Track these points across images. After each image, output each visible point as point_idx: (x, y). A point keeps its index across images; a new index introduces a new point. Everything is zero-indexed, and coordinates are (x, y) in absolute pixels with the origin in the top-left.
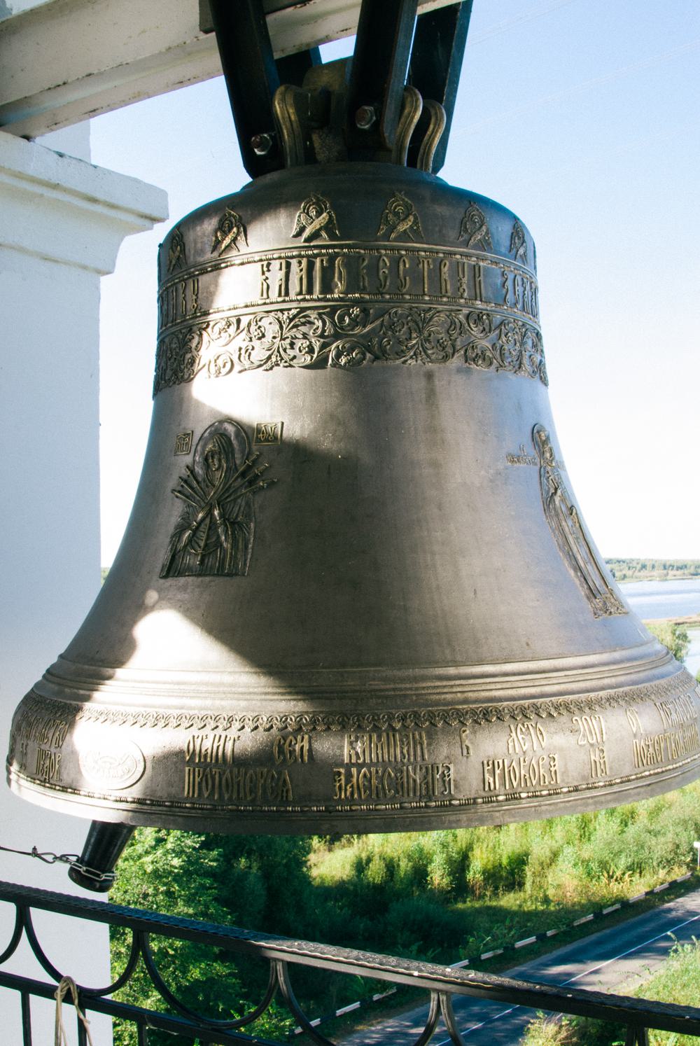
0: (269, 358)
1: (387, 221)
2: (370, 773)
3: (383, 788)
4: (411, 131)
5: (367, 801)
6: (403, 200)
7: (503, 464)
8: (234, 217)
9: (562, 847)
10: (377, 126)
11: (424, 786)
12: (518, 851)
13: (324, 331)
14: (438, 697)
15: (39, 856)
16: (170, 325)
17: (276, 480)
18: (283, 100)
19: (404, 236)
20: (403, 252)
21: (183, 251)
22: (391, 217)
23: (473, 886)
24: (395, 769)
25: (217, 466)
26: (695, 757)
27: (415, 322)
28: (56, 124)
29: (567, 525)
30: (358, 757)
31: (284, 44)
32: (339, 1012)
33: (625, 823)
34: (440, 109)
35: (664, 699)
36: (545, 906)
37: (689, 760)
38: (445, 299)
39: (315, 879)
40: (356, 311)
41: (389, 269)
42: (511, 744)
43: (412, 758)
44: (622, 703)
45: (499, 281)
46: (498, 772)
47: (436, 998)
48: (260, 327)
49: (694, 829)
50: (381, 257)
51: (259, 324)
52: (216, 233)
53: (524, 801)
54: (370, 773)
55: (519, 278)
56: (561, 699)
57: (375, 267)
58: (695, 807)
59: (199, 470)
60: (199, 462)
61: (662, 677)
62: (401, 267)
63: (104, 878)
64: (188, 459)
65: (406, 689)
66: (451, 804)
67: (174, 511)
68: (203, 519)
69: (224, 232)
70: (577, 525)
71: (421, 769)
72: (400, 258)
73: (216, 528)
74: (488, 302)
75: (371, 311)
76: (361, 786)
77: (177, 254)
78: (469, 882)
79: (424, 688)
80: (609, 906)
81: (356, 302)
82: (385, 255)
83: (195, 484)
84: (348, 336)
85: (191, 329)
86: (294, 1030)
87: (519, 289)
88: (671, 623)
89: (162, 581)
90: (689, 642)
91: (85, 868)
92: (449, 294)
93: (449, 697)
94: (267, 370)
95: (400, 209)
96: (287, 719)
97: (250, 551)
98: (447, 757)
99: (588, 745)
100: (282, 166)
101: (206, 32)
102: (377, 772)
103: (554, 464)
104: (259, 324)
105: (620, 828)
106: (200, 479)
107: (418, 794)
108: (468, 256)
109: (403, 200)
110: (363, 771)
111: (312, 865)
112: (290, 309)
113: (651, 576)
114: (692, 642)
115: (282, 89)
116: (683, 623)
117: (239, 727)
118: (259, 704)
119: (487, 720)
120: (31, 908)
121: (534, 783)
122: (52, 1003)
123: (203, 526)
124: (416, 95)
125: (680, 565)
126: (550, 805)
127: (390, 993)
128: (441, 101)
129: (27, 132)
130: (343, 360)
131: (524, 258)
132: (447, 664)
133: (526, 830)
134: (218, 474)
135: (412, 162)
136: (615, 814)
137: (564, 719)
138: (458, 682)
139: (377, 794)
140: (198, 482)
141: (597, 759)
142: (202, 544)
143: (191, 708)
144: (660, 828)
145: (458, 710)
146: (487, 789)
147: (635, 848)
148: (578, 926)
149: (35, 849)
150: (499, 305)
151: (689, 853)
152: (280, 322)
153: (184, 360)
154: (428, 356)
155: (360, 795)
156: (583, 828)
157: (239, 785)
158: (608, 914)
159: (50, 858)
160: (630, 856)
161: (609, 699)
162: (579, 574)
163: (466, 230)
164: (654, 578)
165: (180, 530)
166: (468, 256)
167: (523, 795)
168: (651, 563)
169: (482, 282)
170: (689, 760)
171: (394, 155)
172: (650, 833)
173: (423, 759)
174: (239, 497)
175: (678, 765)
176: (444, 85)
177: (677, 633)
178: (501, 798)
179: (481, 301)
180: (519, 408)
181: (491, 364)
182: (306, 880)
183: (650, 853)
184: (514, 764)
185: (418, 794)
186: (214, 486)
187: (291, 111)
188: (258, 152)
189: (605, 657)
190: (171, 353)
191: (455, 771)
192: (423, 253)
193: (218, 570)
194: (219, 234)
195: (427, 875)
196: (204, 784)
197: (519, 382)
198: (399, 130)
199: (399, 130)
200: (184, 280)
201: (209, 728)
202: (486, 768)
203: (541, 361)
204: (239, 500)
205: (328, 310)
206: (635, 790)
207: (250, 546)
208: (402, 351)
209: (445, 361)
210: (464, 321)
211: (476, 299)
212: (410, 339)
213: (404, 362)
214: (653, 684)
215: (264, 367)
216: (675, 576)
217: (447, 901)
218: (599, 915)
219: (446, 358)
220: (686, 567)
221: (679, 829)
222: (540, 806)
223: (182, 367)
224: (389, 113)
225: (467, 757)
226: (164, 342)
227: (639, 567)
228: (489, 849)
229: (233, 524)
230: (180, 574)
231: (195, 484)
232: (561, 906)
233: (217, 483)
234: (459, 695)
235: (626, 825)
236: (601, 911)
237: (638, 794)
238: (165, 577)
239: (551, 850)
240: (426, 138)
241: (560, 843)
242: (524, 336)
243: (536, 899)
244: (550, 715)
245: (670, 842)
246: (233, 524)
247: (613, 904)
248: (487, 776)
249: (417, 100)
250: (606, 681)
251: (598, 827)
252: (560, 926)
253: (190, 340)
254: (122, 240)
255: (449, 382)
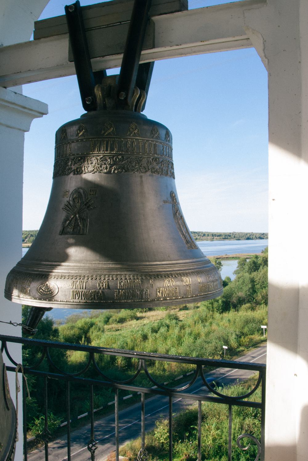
0: (94, 170)
1: (130, 131)
2: (125, 291)
3: (129, 295)
4: (136, 99)
5: (124, 300)
6: (135, 124)
7: (162, 203)
8: (83, 126)
9: (170, 348)
10: (126, 99)
11: (140, 295)
12: (153, 350)
13: (110, 163)
14: (144, 270)
15: (12, 324)
16: (61, 157)
17: (96, 206)
18: (98, 90)
19: (135, 135)
20: (134, 140)
21: (66, 135)
22: (131, 129)
23: (134, 364)
24: (133, 291)
25: (77, 202)
26: (217, 291)
27: (137, 161)
28: (16, 84)
29: (180, 222)
30: (122, 287)
31: (96, 68)
32: (79, 417)
33: (195, 338)
34: (144, 93)
35: (208, 273)
36: (164, 372)
37: (215, 291)
38: (146, 154)
39: (69, 362)
40: (120, 157)
41: (130, 145)
42: (164, 284)
43: (137, 287)
44: (196, 274)
45: (162, 149)
46: (161, 292)
47: (141, 361)
48: (91, 160)
49: (223, 341)
50: (128, 141)
51: (91, 159)
52: (78, 131)
53: (168, 300)
54: (125, 291)
55: (167, 147)
56: (178, 272)
57: (126, 144)
58: (224, 332)
59: (71, 203)
60: (71, 200)
61: (207, 267)
62: (134, 144)
63: (34, 330)
64: (68, 199)
65: (135, 268)
66: (148, 301)
67: (63, 215)
68: (73, 218)
69: (80, 131)
70: (183, 222)
71: (139, 290)
72: (133, 142)
73: (78, 220)
74: (158, 155)
75: (125, 157)
76: (123, 295)
77: (64, 135)
78: (133, 363)
79: (140, 268)
80: (189, 372)
81: (120, 155)
82: (129, 141)
83: (70, 207)
84: (117, 164)
85: (68, 159)
86: (60, 425)
87: (167, 150)
88: (214, 258)
89: (60, 236)
90: (222, 266)
91: (28, 327)
92: (147, 153)
93: (147, 270)
94: (93, 173)
95: (134, 127)
96: (101, 276)
97: (88, 227)
98: (147, 287)
99: (186, 285)
100: (95, 109)
101: (71, 62)
102: (127, 291)
103: (177, 203)
104: (91, 159)
105: (194, 341)
106: (71, 205)
107: (139, 297)
108: (153, 141)
109: (135, 124)
110: (123, 291)
111: (68, 356)
112: (100, 156)
113: (207, 239)
114: (223, 266)
115: (97, 86)
116: (219, 258)
117: (87, 278)
118: (92, 272)
119: (158, 277)
120: (7, 342)
121: (171, 295)
122: (15, 373)
123: (73, 219)
124: (138, 89)
125: (218, 234)
126: (175, 302)
127: (100, 409)
128: (144, 90)
129: (6, 86)
130: (116, 172)
131: (169, 141)
132: (146, 261)
133: (156, 341)
134: (78, 204)
135: (135, 110)
136: (192, 335)
137: (179, 278)
138: (149, 266)
139: (127, 298)
140: (71, 206)
141: (189, 289)
142: (73, 225)
143: (71, 273)
144: (210, 340)
145: (150, 274)
146: (158, 296)
147: (200, 349)
148: (177, 380)
149: (11, 321)
150: (162, 156)
151: (221, 350)
152: (97, 159)
153: (66, 169)
154: (141, 171)
155: (122, 298)
156: (179, 341)
157: (87, 295)
158: (188, 375)
159: (16, 324)
160: (198, 352)
161: (192, 272)
162: (184, 236)
163: (153, 134)
164: (208, 240)
165: (65, 221)
166: (153, 141)
167: (168, 299)
168: (207, 233)
169: (157, 149)
170: (215, 291)
171: (130, 107)
172: (206, 342)
173: (140, 288)
174: (84, 211)
175: (212, 292)
176: (146, 85)
177: (217, 262)
178: (162, 299)
179: (157, 154)
180: (167, 186)
181: (159, 173)
182: (66, 362)
183: (205, 350)
184: (165, 290)
185: (139, 297)
186: (76, 208)
187: (100, 93)
188: (87, 103)
189: (191, 261)
190: (61, 166)
191: (149, 291)
192: (140, 140)
193: (78, 233)
194: (78, 131)
195: (116, 360)
196: (77, 295)
197: (167, 178)
198: (132, 100)
199: (132, 100)
200: (67, 144)
201: (78, 279)
202: (158, 291)
203: (173, 172)
204: (84, 212)
205: (112, 156)
206: (199, 299)
207: (88, 226)
208: (133, 169)
209: (146, 172)
210: (151, 161)
211: (155, 154)
212: (136, 166)
213: (134, 173)
214: (205, 269)
215: (92, 172)
216: (217, 239)
217: (124, 371)
218: (185, 376)
219: (146, 171)
220: (221, 235)
221: (217, 341)
222: (172, 302)
223: (65, 170)
224: (130, 95)
225: (152, 287)
226: (58, 162)
227: (202, 235)
228: (141, 349)
229: (83, 219)
230: (66, 234)
231: (70, 207)
232: (170, 372)
233: (77, 207)
234: (150, 270)
235: (196, 339)
236: (186, 374)
237: (200, 300)
238: (61, 235)
239: (166, 349)
240: (140, 102)
241: (170, 346)
242: (168, 164)
243: (160, 369)
244: (175, 276)
245: (214, 346)
246: (83, 219)
247: (191, 371)
248: (158, 293)
249: (138, 91)
250: (191, 267)
251: (185, 340)
252: (170, 380)
253: (68, 163)
254: (32, 120)
255: (147, 179)
